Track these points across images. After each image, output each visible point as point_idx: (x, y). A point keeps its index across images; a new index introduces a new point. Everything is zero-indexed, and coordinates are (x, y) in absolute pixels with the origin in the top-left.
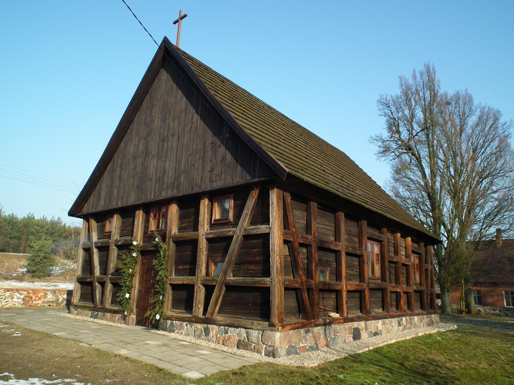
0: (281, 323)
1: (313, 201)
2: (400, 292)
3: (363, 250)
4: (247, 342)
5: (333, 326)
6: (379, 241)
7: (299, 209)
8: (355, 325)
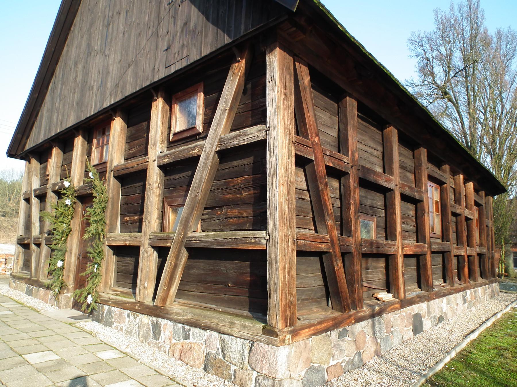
0: (291, 325)
1: (351, 96)
2: (464, 256)
3: (422, 192)
4: (222, 362)
5: (384, 316)
6: (440, 183)
7: (325, 109)
8: (415, 310)
